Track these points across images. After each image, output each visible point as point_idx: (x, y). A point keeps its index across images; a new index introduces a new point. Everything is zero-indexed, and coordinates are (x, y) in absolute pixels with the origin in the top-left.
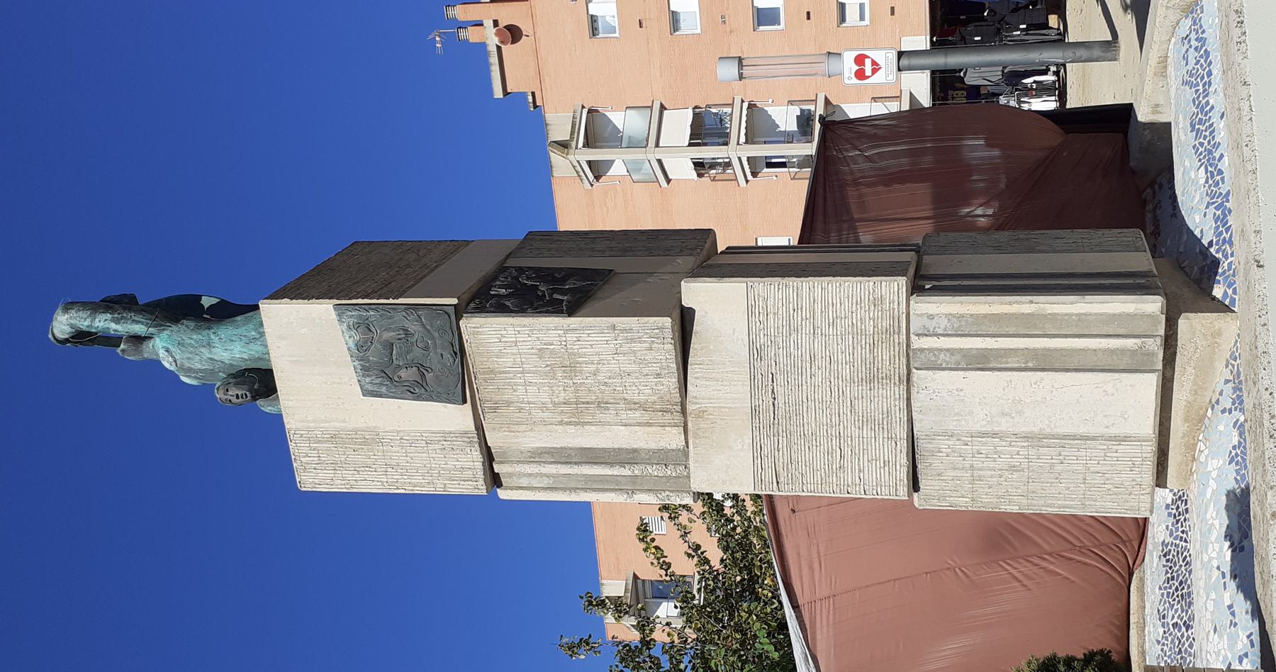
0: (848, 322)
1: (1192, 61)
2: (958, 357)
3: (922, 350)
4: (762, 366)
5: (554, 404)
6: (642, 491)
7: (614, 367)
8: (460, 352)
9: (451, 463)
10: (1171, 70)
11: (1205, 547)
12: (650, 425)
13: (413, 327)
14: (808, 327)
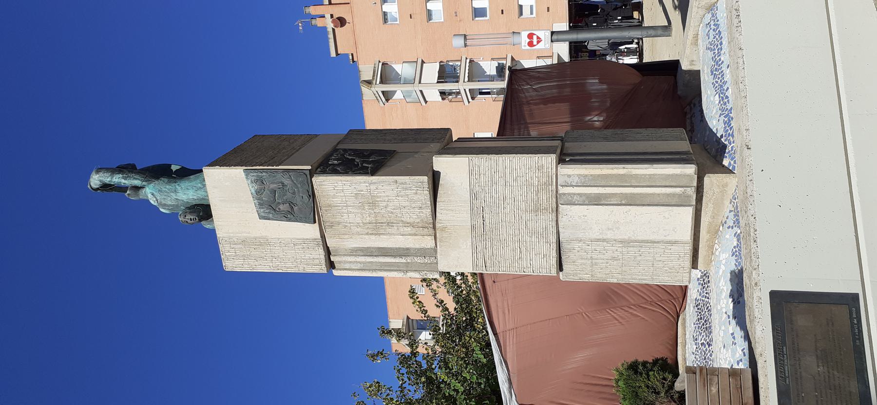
2: (584, 198)
3: (564, 194)
4: (477, 203)
6: (411, 271)
7: (396, 203)
9: (308, 256)
10: (700, 42)
11: (719, 301)
12: (416, 235)
13: (287, 182)
14: (502, 182)
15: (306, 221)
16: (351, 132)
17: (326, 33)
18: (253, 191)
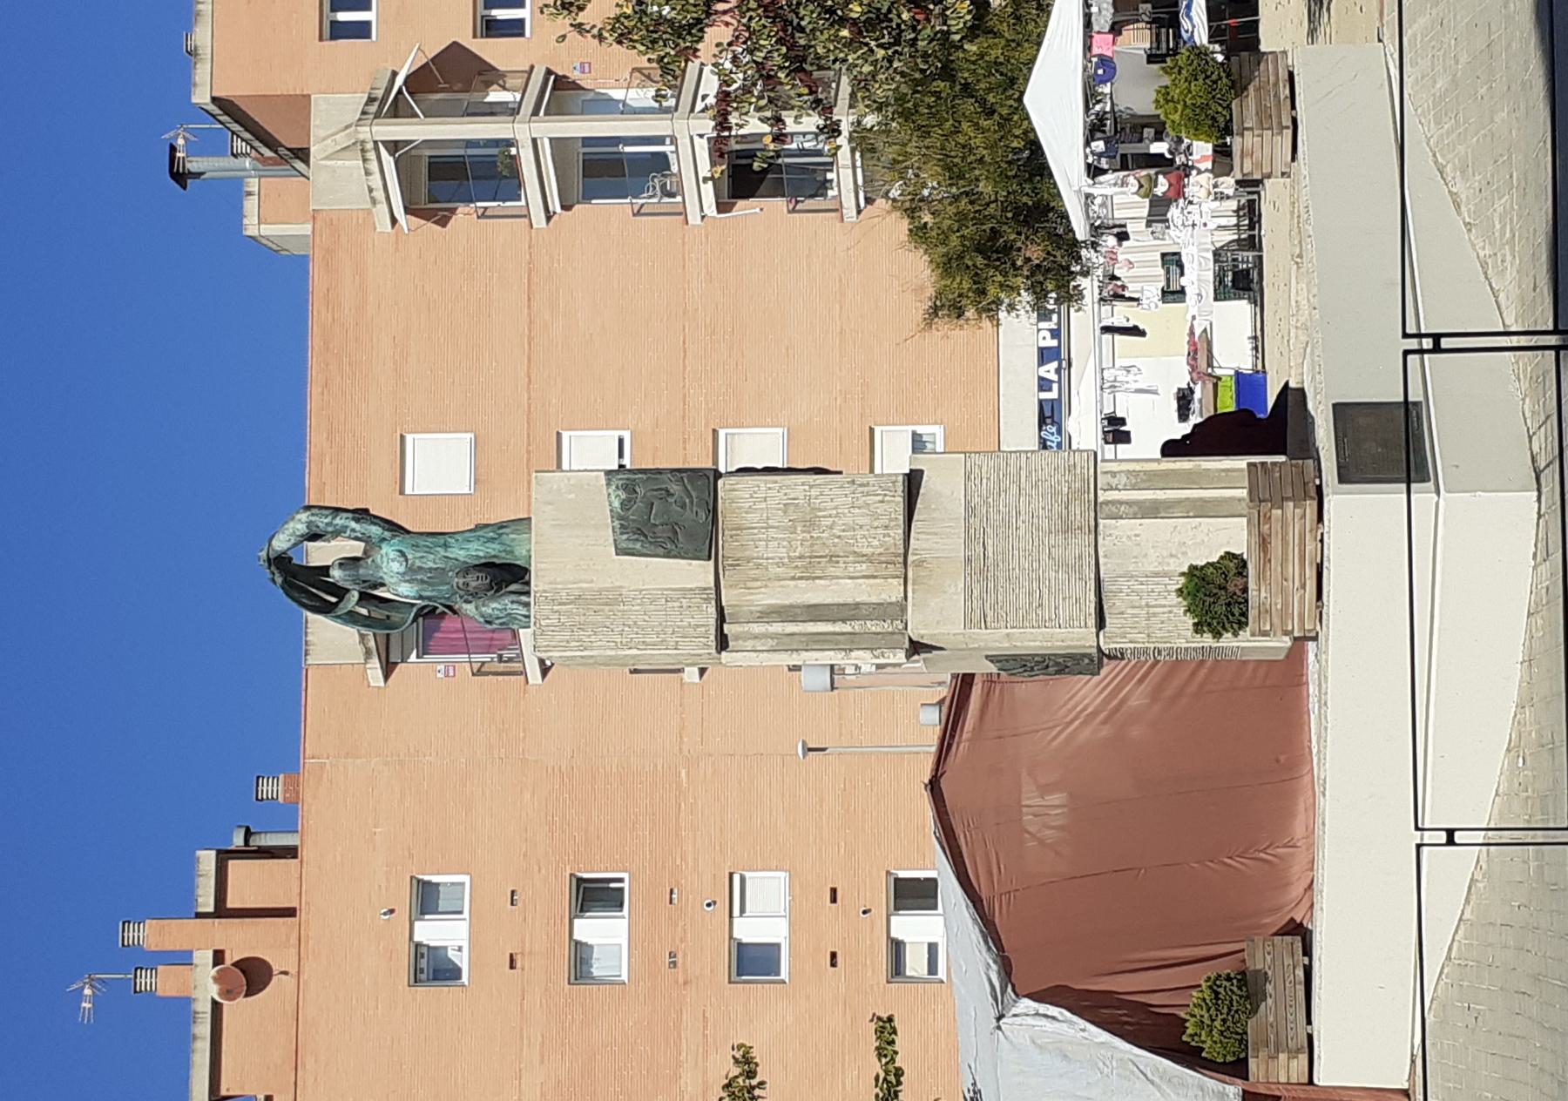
7: (849, 520)
14: (1014, 489)
17: (191, 1017)
18: (616, 504)
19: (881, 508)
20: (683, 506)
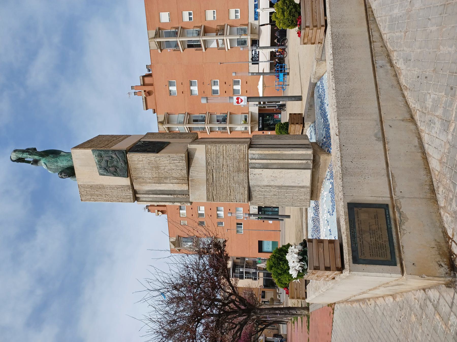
0: (232, 156)
1: (320, 92)
2: (261, 165)
3: (252, 163)
4: (209, 167)
5: (152, 177)
6: (177, 202)
8: (126, 163)
9: (124, 194)
10: (315, 95)
11: (323, 215)
12: (179, 183)
13: (114, 156)
14: (221, 157)
15: (125, 177)
16: (148, 134)
18: (96, 161)
19: (179, 164)
20: (117, 162)
